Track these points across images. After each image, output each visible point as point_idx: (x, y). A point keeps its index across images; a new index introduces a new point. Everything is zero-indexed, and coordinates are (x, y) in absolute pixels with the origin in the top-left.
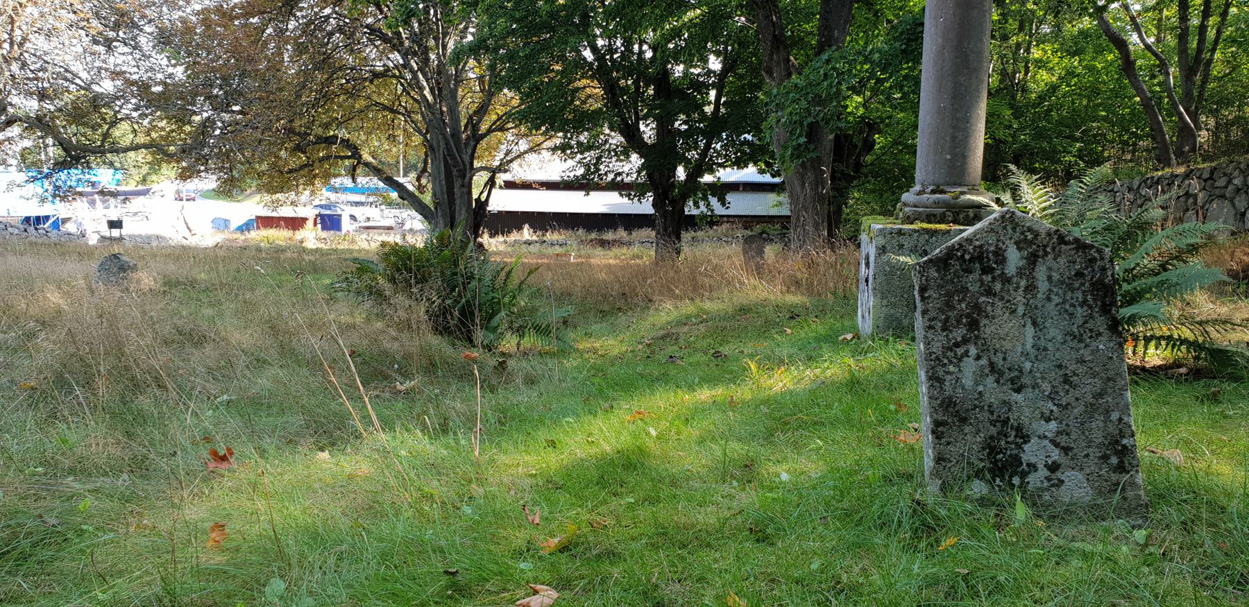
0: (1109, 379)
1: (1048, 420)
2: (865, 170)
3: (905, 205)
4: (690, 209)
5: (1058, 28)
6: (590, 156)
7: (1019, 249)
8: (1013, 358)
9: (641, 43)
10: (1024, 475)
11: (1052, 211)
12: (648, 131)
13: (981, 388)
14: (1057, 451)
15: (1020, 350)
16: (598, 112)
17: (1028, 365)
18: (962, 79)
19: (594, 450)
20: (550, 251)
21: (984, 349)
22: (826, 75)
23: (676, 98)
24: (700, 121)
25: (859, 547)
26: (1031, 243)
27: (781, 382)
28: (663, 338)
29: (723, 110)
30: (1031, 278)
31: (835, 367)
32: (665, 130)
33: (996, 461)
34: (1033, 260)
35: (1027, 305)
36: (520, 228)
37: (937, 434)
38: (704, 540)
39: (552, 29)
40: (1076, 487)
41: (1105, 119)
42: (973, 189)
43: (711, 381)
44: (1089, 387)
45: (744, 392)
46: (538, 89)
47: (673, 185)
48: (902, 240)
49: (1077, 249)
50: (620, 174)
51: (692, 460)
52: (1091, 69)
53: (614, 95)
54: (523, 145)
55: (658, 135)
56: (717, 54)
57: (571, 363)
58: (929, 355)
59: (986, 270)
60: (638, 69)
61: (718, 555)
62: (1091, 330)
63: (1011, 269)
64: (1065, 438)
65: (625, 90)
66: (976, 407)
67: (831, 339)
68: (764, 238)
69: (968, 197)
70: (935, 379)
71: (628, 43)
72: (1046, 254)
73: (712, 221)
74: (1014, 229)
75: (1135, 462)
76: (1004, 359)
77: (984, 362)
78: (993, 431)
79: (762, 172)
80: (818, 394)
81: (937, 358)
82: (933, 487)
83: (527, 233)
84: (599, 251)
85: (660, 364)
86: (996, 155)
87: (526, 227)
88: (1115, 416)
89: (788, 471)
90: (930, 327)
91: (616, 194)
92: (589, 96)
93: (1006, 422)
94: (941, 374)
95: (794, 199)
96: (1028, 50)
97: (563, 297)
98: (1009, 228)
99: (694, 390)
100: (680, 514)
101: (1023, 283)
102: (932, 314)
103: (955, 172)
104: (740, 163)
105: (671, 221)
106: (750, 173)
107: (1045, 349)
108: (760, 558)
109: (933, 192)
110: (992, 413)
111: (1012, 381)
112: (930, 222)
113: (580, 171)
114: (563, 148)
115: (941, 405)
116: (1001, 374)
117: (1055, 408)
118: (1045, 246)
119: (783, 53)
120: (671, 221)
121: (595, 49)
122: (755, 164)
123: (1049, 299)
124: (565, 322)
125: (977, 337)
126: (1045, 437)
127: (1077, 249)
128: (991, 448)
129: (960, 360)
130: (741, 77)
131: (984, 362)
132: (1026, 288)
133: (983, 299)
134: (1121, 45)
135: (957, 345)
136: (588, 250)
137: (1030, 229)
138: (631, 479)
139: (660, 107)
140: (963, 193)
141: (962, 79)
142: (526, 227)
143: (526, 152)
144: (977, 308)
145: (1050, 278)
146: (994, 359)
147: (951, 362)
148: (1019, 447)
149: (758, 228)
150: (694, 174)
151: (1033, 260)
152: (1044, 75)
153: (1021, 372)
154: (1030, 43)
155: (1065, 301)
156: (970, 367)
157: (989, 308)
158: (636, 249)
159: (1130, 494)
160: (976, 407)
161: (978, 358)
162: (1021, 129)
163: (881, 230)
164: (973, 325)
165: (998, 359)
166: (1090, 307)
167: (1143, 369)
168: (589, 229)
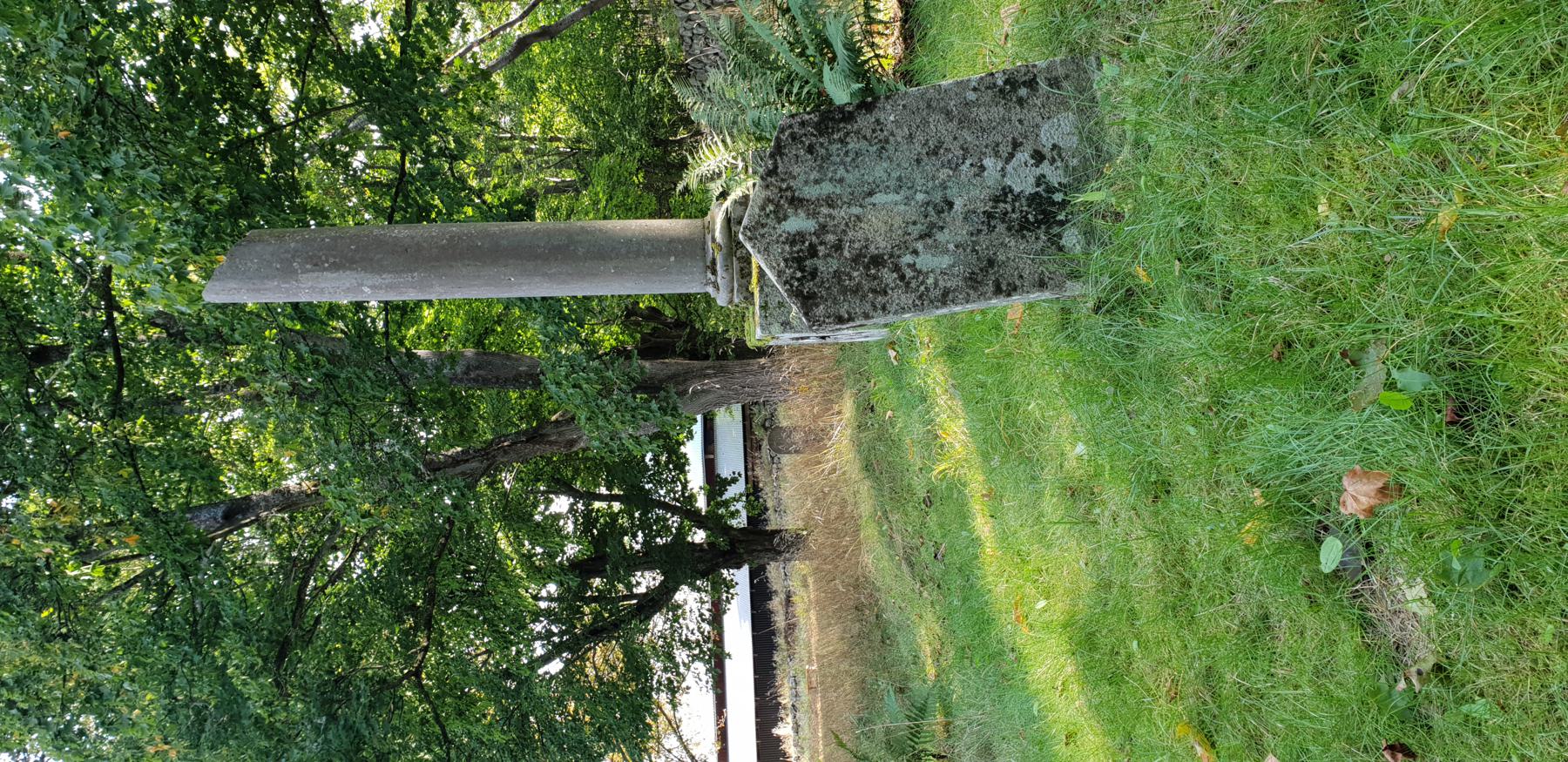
0: (929, 106)
1: (983, 168)
2: (683, 316)
3: (731, 302)
4: (740, 522)
5: (505, 108)
6: (681, 655)
7: (785, 218)
8: (912, 213)
9: (536, 598)
10: (1051, 190)
11: (728, 140)
12: (646, 581)
13: (951, 247)
14: (1019, 155)
15: (902, 207)
16: (623, 647)
17: (920, 197)
18: (581, 251)
19: (1075, 688)
20: (805, 696)
21: (904, 246)
22: (574, 386)
23: (606, 553)
24: (632, 517)
25: (1162, 375)
26: (778, 205)
27: (956, 430)
28: (911, 565)
29: (616, 491)
30: (818, 202)
31: (933, 374)
32: (646, 560)
33: (1036, 221)
34: (797, 202)
35: (849, 204)
36: (778, 740)
37: (1012, 290)
38: (1176, 559)
39: (525, 717)
40: (1058, 130)
41: (607, 50)
42: (709, 228)
43: (964, 517)
44: (939, 127)
45: (976, 483)
46: (600, 729)
47: (711, 545)
48: (773, 303)
49: (781, 155)
50: (701, 615)
51: (1070, 560)
52: (552, 68)
53: (603, 630)
54: (671, 742)
55: (651, 569)
56: (549, 502)
57: (957, 691)
58: (918, 307)
59: (813, 252)
60: (571, 601)
61: (1193, 542)
62: (874, 131)
63: (809, 225)
64: (1001, 148)
65: (597, 616)
66: (974, 250)
67: (898, 375)
68: (770, 425)
69: (718, 235)
70: (945, 298)
71: (537, 615)
72: (789, 188)
73: (754, 491)
74: (763, 226)
75: (1023, 70)
76: (914, 223)
77: (919, 246)
78: (1001, 228)
79: (690, 436)
80: (973, 400)
81: (920, 297)
82: (1074, 288)
83: (783, 730)
84: (801, 635)
85: (946, 572)
86: (656, 166)
87: (776, 731)
88: (971, 96)
89: (1074, 446)
90: (884, 308)
91: (725, 617)
92: (606, 661)
93: (989, 215)
94: (938, 292)
95: (724, 401)
96: (532, 140)
97: (865, 690)
98: (762, 231)
99: (978, 538)
100: (1144, 577)
101: (825, 210)
102: (868, 307)
103: (690, 250)
104: (681, 464)
105: (755, 543)
106: (693, 450)
107: (900, 179)
108: (1189, 492)
109: (714, 272)
110: (979, 231)
111: (940, 212)
112: (750, 274)
113: (700, 667)
114: (673, 690)
115: (975, 289)
116: (932, 225)
117: (968, 162)
118: (781, 190)
119: (548, 429)
120: (755, 543)
121: (546, 659)
122: (680, 444)
123: (841, 181)
124: (901, 691)
125: (891, 256)
126: (1003, 169)
127: (781, 155)
128: (1023, 228)
129: (920, 272)
130: (576, 471)
131: (919, 246)
132: (830, 206)
133: (846, 254)
134: (524, 43)
135: (902, 277)
136: (801, 651)
137: (763, 208)
138: (1105, 641)
139: (615, 569)
140: (714, 240)
141: (581, 251)
142: (776, 731)
143: (680, 738)
144: (856, 259)
145: (817, 182)
146: (915, 234)
147: (923, 283)
148: (1017, 197)
149: (759, 433)
150: (699, 520)
151: (797, 202)
152: (560, 121)
153: (928, 204)
154: (523, 138)
155: (843, 163)
156: (926, 261)
157: (857, 245)
158: (795, 584)
159: (1061, 71)
160: (974, 250)
161: (915, 252)
162: (624, 141)
163: (763, 329)
164: (877, 261)
165: (915, 231)
166: (848, 134)
167: (905, 21)
168: (773, 647)
